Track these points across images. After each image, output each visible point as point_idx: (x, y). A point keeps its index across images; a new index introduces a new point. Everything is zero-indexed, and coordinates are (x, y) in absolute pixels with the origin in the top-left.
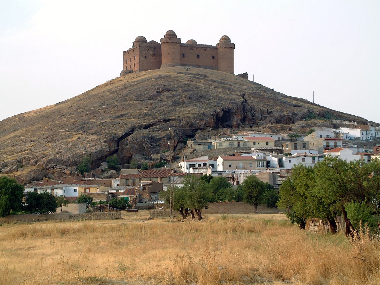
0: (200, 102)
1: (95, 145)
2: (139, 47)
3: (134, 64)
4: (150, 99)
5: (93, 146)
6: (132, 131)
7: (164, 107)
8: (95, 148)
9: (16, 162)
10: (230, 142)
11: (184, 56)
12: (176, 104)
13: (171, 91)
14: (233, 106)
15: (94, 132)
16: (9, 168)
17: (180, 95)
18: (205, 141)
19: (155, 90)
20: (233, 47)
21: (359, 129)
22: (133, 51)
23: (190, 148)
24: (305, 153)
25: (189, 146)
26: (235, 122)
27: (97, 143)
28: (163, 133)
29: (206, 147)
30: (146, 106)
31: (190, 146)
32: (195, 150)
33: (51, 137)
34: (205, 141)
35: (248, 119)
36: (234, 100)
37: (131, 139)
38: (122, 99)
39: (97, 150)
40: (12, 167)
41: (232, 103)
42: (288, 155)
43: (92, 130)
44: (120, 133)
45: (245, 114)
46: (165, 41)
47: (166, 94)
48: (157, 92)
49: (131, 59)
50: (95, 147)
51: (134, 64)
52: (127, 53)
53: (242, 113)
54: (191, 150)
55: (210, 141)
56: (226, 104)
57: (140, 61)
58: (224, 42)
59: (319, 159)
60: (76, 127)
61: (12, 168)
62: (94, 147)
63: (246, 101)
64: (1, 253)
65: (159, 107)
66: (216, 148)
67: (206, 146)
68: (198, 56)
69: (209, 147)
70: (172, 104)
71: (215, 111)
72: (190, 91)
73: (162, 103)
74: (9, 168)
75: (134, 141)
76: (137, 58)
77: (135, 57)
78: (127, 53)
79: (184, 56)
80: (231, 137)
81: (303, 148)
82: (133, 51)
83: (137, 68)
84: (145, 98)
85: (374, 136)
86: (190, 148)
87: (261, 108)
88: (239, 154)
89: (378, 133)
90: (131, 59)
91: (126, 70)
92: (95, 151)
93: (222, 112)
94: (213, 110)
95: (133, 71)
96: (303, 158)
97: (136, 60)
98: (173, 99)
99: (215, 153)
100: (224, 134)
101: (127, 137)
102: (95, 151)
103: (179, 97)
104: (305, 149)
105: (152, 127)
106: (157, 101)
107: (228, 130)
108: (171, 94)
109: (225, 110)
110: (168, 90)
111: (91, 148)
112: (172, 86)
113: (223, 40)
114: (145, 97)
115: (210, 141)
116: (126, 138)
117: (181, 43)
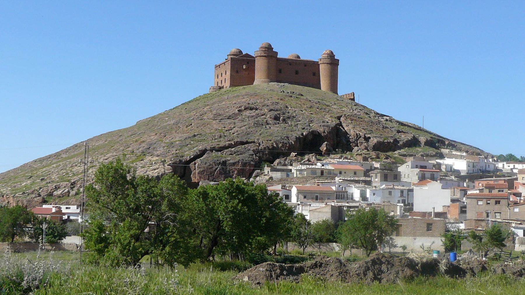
0: (286, 123)
1: (158, 169)
2: (230, 61)
3: (225, 79)
4: (230, 119)
5: (155, 170)
6: (203, 153)
7: (244, 128)
8: (157, 172)
9: (69, 185)
10: (312, 169)
11: (280, 71)
12: (258, 124)
13: (254, 110)
14: (324, 129)
15: (159, 154)
16: (61, 191)
17: (265, 114)
18: (285, 168)
19: (236, 108)
20: (337, 63)
21: (465, 160)
22: (225, 65)
23: (266, 175)
24: (392, 186)
25: (266, 173)
26: (324, 147)
27: (160, 166)
28: (238, 157)
29: (284, 174)
30: (224, 125)
31: (267, 173)
32: (271, 178)
33: (113, 158)
34: (285, 168)
35: (342, 144)
36: (327, 122)
37: (200, 163)
38: (198, 118)
39: (159, 174)
40: (64, 189)
41: (324, 126)
42: (494, 177)
43: (158, 151)
44: (189, 154)
45: (339, 139)
46: (259, 54)
47: (248, 113)
48: (238, 111)
49: (222, 74)
50: (157, 170)
51: (225, 79)
52: (224, 64)
53: (335, 137)
54: (267, 178)
55: (290, 167)
56: (317, 127)
57: (232, 76)
58: (326, 57)
59: (408, 193)
60: (141, 147)
61: (63, 191)
62: (156, 171)
63: (340, 124)
64: (443, 294)
65: (238, 127)
66: (295, 176)
67: (285, 174)
68: (297, 73)
69: (288, 176)
70: (254, 125)
71: (302, 134)
72: (277, 110)
73: (242, 123)
74: (61, 191)
75: (203, 165)
76: (229, 73)
77: (226, 72)
78: (224, 64)
79: (280, 71)
80: (316, 165)
81: (394, 179)
82: (225, 65)
83: (227, 84)
84: (224, 117)
85: (484, 169)
86: (266, 175)
87: (358, 132)
88: (319, 184)
89: (489, 165)
90: (222, 74)
91: (216, 85)
92: (156, 175)
93: (311, 135)
94: (299, 133)
95: (223, 87)
96: (389, 191)
97: (227, 74)
98: (256, 120)
99: (293, 182)
100: (309, 160)
101: (195, 161)
102: (156, 175)
103: (262, 117)
104: (396, 180)
105: (225, 150)
106: (236, 121)
107: (313, 156)
108: (253, 113)
109: (314, 133)
110: (251, 109)
111: (153, 171)
112: (257, 104)
113: (326, 55)
114: (225, 116)
115: (290, 167)
116: (194, 162)
117: (278, 57)
